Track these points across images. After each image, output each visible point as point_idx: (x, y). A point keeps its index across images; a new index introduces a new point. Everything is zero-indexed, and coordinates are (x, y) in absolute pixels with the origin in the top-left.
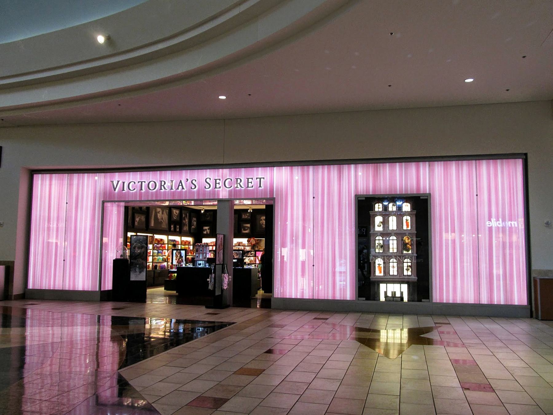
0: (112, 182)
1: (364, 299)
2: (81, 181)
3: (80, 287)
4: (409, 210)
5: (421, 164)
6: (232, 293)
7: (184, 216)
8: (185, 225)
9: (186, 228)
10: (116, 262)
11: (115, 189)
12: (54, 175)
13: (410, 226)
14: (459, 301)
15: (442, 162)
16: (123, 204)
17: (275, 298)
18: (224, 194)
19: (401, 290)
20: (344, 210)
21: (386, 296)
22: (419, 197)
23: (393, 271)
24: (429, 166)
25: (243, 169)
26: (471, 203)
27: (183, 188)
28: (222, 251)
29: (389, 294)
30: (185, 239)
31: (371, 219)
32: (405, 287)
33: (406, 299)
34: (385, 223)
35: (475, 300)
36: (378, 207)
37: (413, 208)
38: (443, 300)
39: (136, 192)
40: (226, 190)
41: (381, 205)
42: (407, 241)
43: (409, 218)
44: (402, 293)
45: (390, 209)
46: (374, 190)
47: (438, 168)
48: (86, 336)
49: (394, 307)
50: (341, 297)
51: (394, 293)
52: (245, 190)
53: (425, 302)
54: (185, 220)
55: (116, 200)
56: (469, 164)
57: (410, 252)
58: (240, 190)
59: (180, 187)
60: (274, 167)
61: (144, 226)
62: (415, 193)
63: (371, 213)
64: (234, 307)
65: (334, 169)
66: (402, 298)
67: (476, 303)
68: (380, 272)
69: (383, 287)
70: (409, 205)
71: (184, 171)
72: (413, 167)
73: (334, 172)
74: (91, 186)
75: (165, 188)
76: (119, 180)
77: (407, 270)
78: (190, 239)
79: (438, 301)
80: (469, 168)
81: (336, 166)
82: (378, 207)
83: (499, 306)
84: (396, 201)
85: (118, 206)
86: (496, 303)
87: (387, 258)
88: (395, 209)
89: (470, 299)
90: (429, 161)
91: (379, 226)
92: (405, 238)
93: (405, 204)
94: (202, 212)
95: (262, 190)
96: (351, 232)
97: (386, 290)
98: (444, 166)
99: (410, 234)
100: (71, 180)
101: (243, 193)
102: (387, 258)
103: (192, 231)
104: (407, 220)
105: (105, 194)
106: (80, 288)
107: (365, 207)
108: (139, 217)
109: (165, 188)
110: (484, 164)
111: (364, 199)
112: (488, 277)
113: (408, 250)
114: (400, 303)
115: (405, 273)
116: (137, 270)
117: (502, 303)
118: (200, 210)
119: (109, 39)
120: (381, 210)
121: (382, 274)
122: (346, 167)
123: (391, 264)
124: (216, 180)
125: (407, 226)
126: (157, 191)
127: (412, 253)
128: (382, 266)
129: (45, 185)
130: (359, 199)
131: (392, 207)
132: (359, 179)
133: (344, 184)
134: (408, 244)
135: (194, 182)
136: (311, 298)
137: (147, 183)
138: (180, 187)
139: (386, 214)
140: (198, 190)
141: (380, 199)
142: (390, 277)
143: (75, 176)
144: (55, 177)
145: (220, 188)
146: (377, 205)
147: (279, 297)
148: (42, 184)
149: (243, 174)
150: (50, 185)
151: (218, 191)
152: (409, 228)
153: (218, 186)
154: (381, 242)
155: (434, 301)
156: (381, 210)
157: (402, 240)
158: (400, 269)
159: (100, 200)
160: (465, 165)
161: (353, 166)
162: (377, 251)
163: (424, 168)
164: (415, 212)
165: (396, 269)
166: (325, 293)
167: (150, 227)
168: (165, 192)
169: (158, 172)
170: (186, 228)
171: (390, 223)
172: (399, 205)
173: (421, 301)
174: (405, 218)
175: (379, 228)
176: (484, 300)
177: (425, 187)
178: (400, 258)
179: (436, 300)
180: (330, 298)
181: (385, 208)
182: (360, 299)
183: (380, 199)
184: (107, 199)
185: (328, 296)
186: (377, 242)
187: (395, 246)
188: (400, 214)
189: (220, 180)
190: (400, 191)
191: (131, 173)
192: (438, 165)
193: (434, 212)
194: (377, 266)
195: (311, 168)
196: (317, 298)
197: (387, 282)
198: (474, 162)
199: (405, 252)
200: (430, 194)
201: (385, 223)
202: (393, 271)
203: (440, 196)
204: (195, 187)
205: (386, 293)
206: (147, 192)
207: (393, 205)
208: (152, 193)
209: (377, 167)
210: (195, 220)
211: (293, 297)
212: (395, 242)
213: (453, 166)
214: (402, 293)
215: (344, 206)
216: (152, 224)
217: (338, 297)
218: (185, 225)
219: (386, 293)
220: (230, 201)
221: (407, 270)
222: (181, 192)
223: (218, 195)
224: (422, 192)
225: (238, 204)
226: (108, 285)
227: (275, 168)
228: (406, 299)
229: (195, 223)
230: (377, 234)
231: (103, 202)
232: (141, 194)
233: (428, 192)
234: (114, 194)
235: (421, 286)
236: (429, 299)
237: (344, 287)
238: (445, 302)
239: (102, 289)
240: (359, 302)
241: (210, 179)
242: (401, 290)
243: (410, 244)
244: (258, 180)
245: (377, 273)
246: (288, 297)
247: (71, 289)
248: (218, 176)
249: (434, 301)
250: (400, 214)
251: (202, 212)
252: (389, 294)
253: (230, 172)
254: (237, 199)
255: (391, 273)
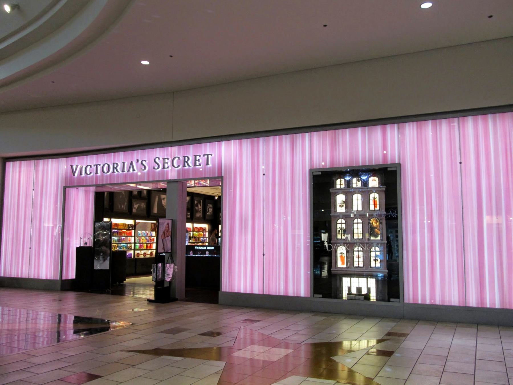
0: (72, 166)
1: (321, 296)
2: (46, 167)
3: (43, 276)
4: (377, 186)
5: (388, 127)
6: (80, 293)
7: (196, 202)
8: (197, 211)
9: (199, 215)
10: (79, 250)
11: (74, 174)
12: (23, 162)
13: (378, 206)
14: (438, 302)
15: (415, 123)
16: (92, 189)
17: (223, 292)
18: (172, 174)
19: (369, 286)
20: (297, 188)
21: (350, 293)
22: (387, 168)
23: (359, 262)
24: (399, 128)
25: (191, 146)
26: (453, 172)
27: (134, 170)
28: (170, 237)
29: (354, 291)
30: (197, 225)
31: (332, 197)
32: (372, 283)
33: (373, 296)
34: (348, 203)
35: (459, 301)
36: (340, 183)
37: (381, 183)
38: (418, 300)
39: (93, 176)
40: (175, 170)
41: (343, 180)
42: (375, 225)
43: (377, 195)
44: (369, 290)
45: (354, 185)
46: (332, 162)
47: (410, 130)
48: (48, 325)
49: (358, 309)
50: (294, 293)
51: (359, 289)
52: (193, 168)
53: (394, 303)
54: (197, 206)
55: (75, 185)
56: (449, 123)
57: (379, 238)
58: (188, 170)
59: (131, 169)
60: (222, 141)
61: (145, 213)
62: (381, 163)
63: (332, 190)
64: (187, 301)
65: (286, 139)
66: (367, 297)
67: (461, 305)
68: (343, 263)
69: (346, 281)
70: (377, 179)
71: (135, 151)
72: (378, 131)
73: (286, 143)
74: (54, 170)
75: (118, 171)
76: (87, 166)
77: (376, 260)
78: (205, 226)
79: (411, 301)
80: (450, 126)
81: (288, 136)
82: (340, 183)
83: (493, 311)
84: (360, 175)
85: (87, 193)
86: (488, 306)
87: (350, 246)
88: (359, 185)
89: (453, 299)
90: (398, 123)
91: (340, 206)
92: (373, 221)
93: (371, 179)
94: (216, 198)
95: (210, 168)
96: (305, 213)
97: (350, 285)
98: (417, 128)
99: (379, 218)
100: (37, 166)
101: (191, 173)
102: (350, 246)
103: (207, 218)
104: (374, 198)
105: (66, 178)
106: (44, 277)
107: (322, 184)
108: (106, 203)
109: (118, 171)
110: (470, 122)
111: (320, 173)
112: (478, 270)
113: (376, 237)
114: (366, 301)
115: (373, 264)
116: (101, 258)
117: (497, 306)
118: (214, 197)
119: (14, 7)
120: (343, 186)
121: (345, 266)
122: (299, 136)
123: (356, 254)
124: (164, 159)
125: (375, 204)
126: (111, 174)
127: (381, 240)
128: (345, 255)
129: (16, 172)
130: (315, 174)
131: (356, 183)
132: (316, 150)
133: (298, 158)
134: (376, 228)
135: (144, 162)
136: (261, 293)
137: (102, 165)
138: (131, 169)
139: (349, 191)
140: (149, 171)
141: (341, 173)
142: (353, 269)
143: (41, 162)
144: (24, 163)
145: (168, 167)
146: (338, 181)
147: (227, 291)
148: (13, 172)
149: (191, 150)
150: (20, 172)
151: (167, 172)
152: (378, 208)
153: (166, 166)
154: (344, 226)
155: (406, 301)
156: (343, 186)
157: (369, 223)
158: (367, 260)
159: (62, 186)
160: (444, 125)
161: (307, 135)
162: (339, 237)
163: (392, 132)
164: (384, 188)
165: (361, 260)
166: (278, 288)
167: (152, 214)
168: (118, 175)
169: (112, 154)
170: (199, 215)
171: (356, 203)
172: (364, 180)
173: (389, 301)
174: (372, 196)
175: (340, 210)
176: (473, 302)
177: (392, 155)
178: (366, 245)
179: (409, 299)
180: (282, 293)
181: (349, 184)
182: (316, 295)
183: (341, 173)
184: (69, 185)
185: (279, 292)
186: (339, 226)
187: (360, 230)
188: (365, 190)
189: (168, 159)
190: (362, 163)
191: (89, 156)
192: (409, 126)
193: (405, 185)
194: (339, 255)
195: (261, 139)
196: (267, 294)
197: (350, 275)
198: (456, 120)
199: (372, 238)
200: (399, 164)
201: (348, 203)
202: (359, 262)
203: (413, 166)
204: (158, 168)
205: (350, 289)
206: (102, 176)
207: (358, 180)
208: (107, 176)
209: (335, 134)
210: (141, 203)
211: (242, 292)
212: (360, 226)
213: (429, 126)
214: (369, 290)
215: (297, 183)
216: (155, 210)
217: (291, 293)
218: (197, 211)
219: (350, 289)
220: (180, 183)
221: (376, 260)
222: (132, 174)
223: (167, 175)
224: (389, 162)
225: (193, 186)
226: (72, 274)
227: (223, 142)
228: (373, 296)
229: (211, 210)
230: (338, 216)
231: (65, 188)
232: (97, 178)
233: (397, 162)
234: (74, 178)
235: (391, 283)
236: (399, 298)
237: (296, 282)
238: (420, 302)
239: (64, 278)
240: (316, 299)
241: (159, 158)
242: (369, 286)
243: (378, 228)
244: (206, 156)
245: (340, 265)
246: (236, 291)
247: (36, 278)
248: (167, 155)
249: (406, 301)
250: (365, 190)
251: (216, 198)
252: (354, 291)
253: (178, 149)
254: (191, 179)
255: (356, 265)
